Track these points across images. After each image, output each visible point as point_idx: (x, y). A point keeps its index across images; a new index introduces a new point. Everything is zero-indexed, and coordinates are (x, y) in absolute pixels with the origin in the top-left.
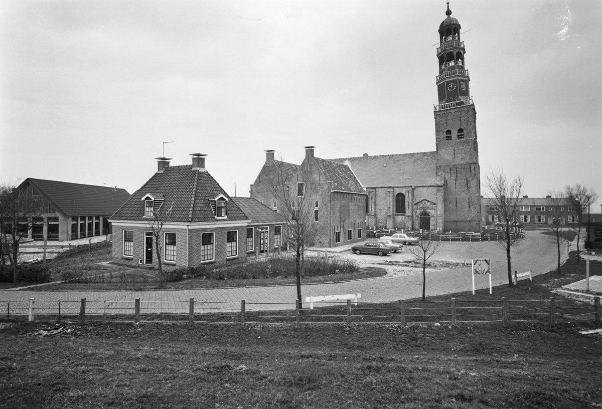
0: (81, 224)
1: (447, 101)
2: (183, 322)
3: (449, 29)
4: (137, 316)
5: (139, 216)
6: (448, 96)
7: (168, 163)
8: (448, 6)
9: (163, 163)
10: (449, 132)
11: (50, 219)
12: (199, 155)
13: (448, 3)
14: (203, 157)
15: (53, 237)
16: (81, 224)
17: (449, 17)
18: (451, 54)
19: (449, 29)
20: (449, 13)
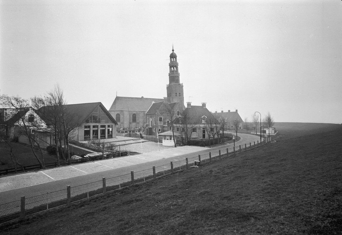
0: (93, 130)
2: (64, 206)
3: (173, 56)
4: (155, 175)
5: (201, 123)
7: (191, 104)
9: (204, 105)
10: (176, 93)
11: (94, 127)
12: (204, 103)
13: (173, 47)
15: (87, 138)
16: (93, 130)
17: (173, 52)
18: (173, 65)
19: (173, 56)
20: (173, 50)
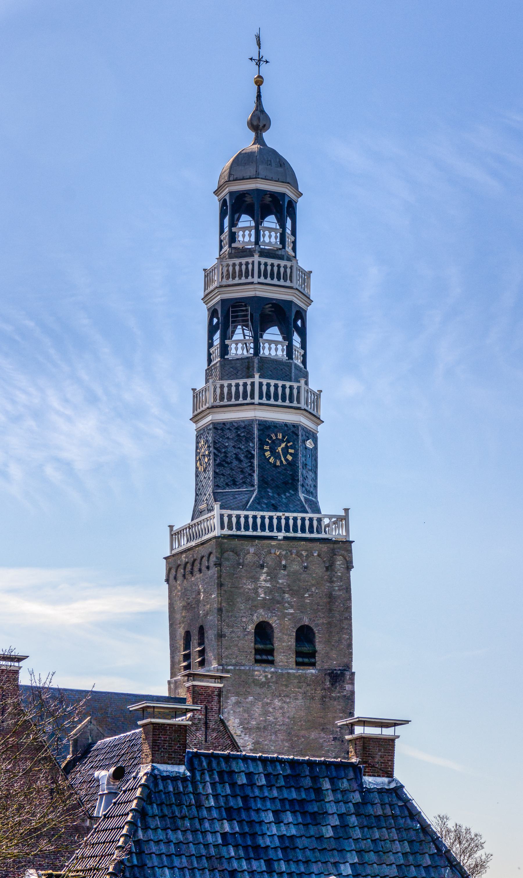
1: (257, 505)
3: (259, 197)
6: (264, 483)
8: (259, 92)
14: (388, 732)
19: (259, 197)
20: (259, 123)
